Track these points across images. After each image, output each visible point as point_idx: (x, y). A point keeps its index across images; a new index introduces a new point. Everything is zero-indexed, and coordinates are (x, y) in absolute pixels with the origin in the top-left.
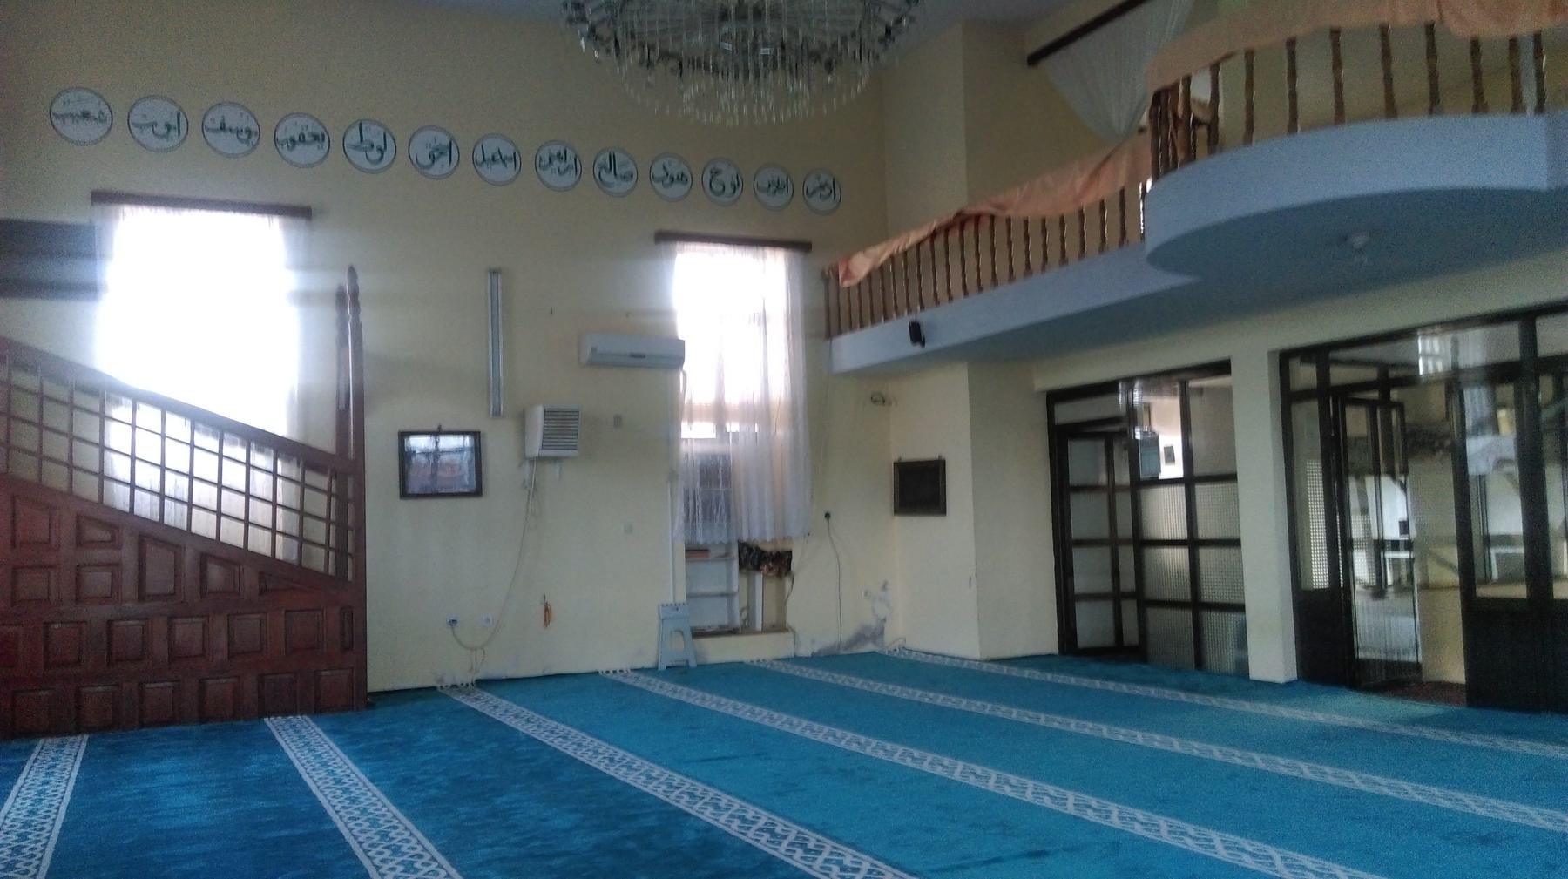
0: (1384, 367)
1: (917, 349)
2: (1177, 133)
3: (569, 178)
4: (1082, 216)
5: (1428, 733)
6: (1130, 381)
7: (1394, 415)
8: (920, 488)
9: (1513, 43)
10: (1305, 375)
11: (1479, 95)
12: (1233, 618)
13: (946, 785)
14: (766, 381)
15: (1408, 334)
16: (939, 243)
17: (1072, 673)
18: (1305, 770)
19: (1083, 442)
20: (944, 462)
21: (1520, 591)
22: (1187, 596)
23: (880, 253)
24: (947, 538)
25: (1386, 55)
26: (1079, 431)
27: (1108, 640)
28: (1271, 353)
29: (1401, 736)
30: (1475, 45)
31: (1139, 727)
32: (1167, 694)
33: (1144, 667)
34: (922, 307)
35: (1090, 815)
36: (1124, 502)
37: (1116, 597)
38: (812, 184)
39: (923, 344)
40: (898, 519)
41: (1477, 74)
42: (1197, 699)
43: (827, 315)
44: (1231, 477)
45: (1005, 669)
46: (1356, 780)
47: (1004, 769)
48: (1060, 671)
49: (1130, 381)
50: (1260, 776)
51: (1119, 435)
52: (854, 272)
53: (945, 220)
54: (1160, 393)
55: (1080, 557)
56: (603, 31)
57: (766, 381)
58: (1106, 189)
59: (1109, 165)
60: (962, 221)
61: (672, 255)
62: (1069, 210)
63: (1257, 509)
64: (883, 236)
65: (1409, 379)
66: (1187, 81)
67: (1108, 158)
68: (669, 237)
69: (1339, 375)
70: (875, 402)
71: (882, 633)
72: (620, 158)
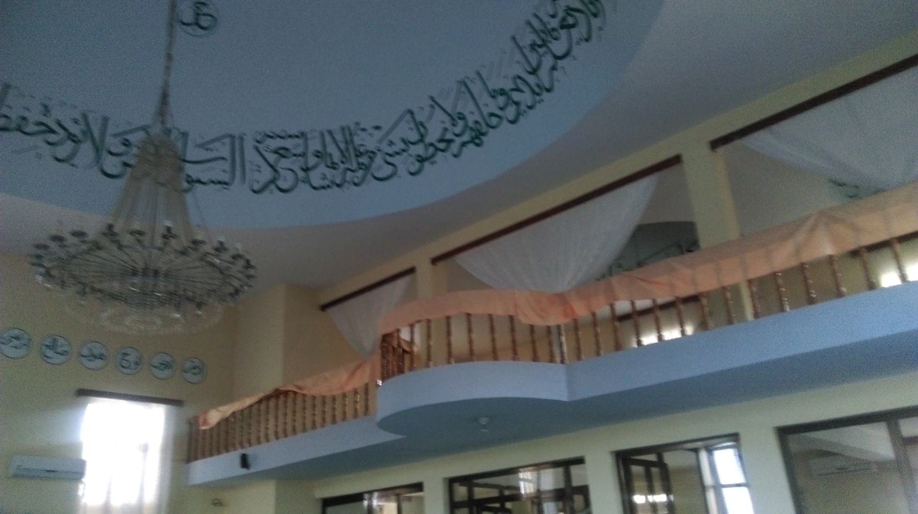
0: (501, 488)
1: (244, 471)
2: (395, 357)
3: (22, 352)
6: (371, 492)
9: (549, 329)
10: (461, 492)
11: (535, 352)
14: (142, 489)
15: (513, 471)
23: (227, 410)
25: (492, 329)
28: (445, 479)
38: (188, 365)
41: (533, 342)
43: (189, 446)
49: (371, 492)
53: (268, 393)
54: (388, 500)
56: (54, 272)
57: (142, 489)
58: (358, 383)
60: (278, 394)
61: (84, 405)
62: (337, 392)
64: (229, 400)
65: (516, 497)
66: (398, 331)
68: (86, 393)
69: (480, 493)
72: (61, 341)
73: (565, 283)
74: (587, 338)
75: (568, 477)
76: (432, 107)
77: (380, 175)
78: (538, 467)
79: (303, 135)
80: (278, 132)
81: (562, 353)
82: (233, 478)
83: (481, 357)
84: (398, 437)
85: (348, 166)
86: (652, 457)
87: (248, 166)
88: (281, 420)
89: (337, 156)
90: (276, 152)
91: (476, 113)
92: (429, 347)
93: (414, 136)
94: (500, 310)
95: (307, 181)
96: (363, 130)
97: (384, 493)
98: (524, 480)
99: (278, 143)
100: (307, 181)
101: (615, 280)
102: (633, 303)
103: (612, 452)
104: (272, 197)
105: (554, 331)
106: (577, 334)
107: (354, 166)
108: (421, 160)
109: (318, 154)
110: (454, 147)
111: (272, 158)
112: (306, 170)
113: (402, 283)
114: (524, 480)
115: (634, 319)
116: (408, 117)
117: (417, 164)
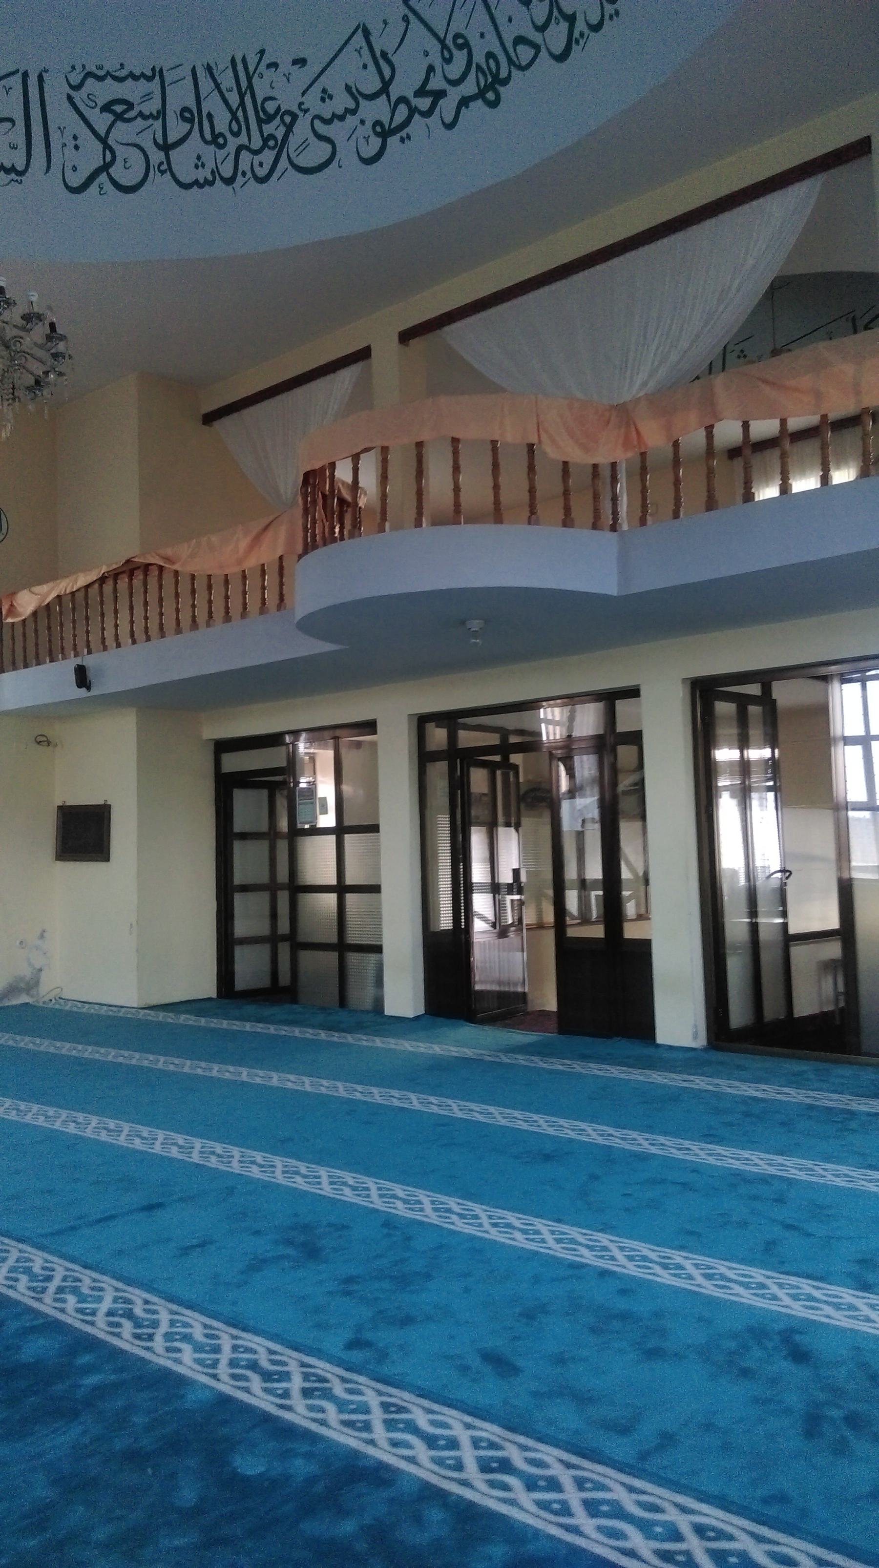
0: (504, 733)
1: (82, 692)
2: (328, 510)
4: (244, 577)
5: (521, 1060)
6: (296, 733)
7: (511, 774)
8: (83, 833)
10: (438, 736)
11: (567, 510)
12: (373, 957)
13: (74, 1143)
15: (532, 705)
16: (108, 588)
17: (226, 1017)
18: (415, 1101)
19: (248, 791)
20: (110, 806)
21: (598, 932)
22: (334, 939)
23: (48, 592)
24: (110, 885)
26: (245, 780)
27: (265, 982)
29: (501, 1064)
30: (193, 577)
31: (276, 1069)
32: (309, 1033)
33: (295, 1006)
34: (90, 652)
35: (213, 1162)
36: (282, 846)
37: (273, 939)
39: (89, 688)
40: (59, 864)
41: (566, 493)
42: (336, 1037)
44: (374, 828)
45: (161, 1016)
46: (456, 1109)
47: (252, 1067)
48: (216, 1015)
49: (296, 733)
50: (377, 1110)
51: (280, 783)
52: (20, 609)
55: (239, 901)
58: (267, 553)
59: (270, 534)
60: (130, 568)
62: (233, 570)
63: (393, 859)
64: (53, 576)
65: (530, 744)
66: (333, 466)
67: (266, 528)
69: (467, 739)
70: (39, 743)
71: (37, 983)
73: (634, 386)
74: (660, 490)
75: (610, 717)
76: (406, 19)
77: (302, 161)
78: (571, 699)
79: (157, 74)
80: (111, 65)
81: (615, 513)
82: (70, 702)
83: (473, 519)
84: (326, 647)
85: (243, 139)
86: (754, 689)
87: (54, 136)
88: (139, 610)
89: (222, 122)
90: (106, 108)
91: (491, 36)
92: (384, 497)
93: (372, 84)
94: (511, 434)
95: (167, 168)
96: (274, 65)
97: (316, 734)
98: (548, 722)
99: (107, 91)
100: (167, 168)
101: (719, 380)
102: (746, 426)
103: (684, 680)
104: (101, 201)
105: (606, 473)
106: (643, 480)
107: (256, 143)
108: (384, 132)
109: (185, 114)
110: (447, 106)
111: (101, 122)
112: (166, 147)
113: (347, 377)
114: (548, 722)
115: (749, 453)
116: (359, 37)
117: (376, 142)
